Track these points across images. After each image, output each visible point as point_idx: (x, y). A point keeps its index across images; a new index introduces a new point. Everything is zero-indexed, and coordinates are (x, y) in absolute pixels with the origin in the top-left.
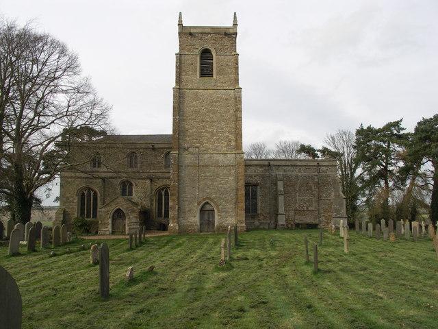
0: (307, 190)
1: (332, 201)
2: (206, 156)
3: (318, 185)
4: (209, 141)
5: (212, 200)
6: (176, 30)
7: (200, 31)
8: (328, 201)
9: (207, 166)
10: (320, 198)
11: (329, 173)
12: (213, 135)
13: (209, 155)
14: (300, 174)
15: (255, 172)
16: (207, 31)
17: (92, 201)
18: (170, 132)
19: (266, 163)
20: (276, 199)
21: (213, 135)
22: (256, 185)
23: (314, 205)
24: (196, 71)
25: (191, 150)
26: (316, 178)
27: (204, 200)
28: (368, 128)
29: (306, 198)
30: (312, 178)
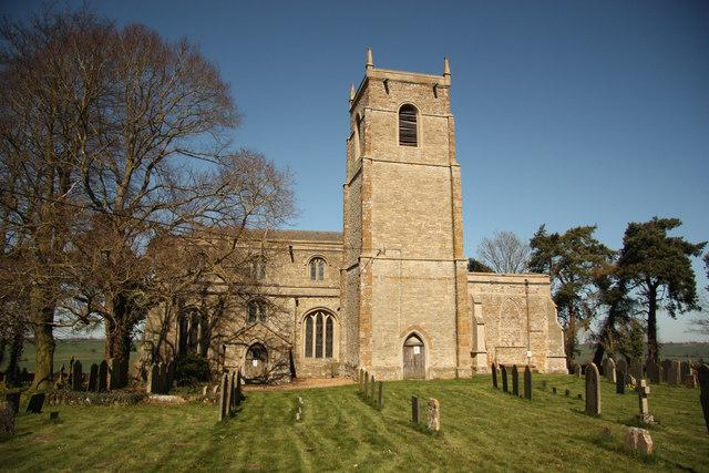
25: (389, 253)
26: (524, 301)
27: (410, 329)
29: (511, 330)
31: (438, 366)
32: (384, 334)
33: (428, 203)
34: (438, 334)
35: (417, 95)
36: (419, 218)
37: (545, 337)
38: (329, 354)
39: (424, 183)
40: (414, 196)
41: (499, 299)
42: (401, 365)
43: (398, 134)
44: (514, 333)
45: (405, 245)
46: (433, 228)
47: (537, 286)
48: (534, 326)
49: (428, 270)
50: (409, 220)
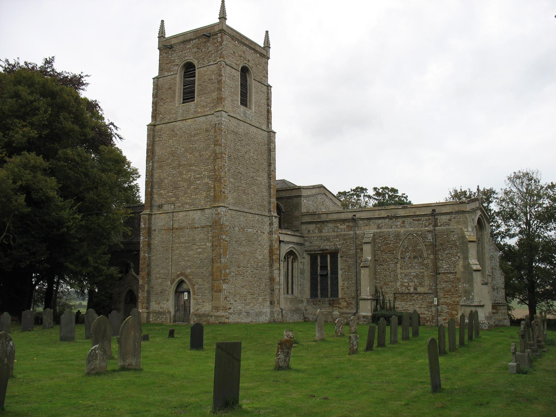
0: (415, 257)
1: (458, 276)
2: (181, 215)
3: (434, 248)
4: (186, 193)
5: (186, 277)
6: (155, 42)
7: (181, 39)
8: (451, 276)
9: (181, 228)
10: (436, 272)
11: (453, 226)
12: (190, 183)
13: (184, 213)
14: (402, 230)
15: (334, 231)
16: (188, 38)
17: (319, 288)
18: (277, 179)
19: (429, 211)
20: (358, 275)
21: (190, 183)
22: (334, 255)
23: (427, 282)
24: (174, 97)
25: (166, 207)
26: (430, 236)
27: (178, 276)
28: (125, 157)
29: (413, 272)
30: (423, 236)
31: (199, 312)
32: (160, 281)
33: (197, 154)
34: (200, 281)
35: (195, 50)
36: (189, 171)
37: (459, 279)
38: (292, 293)
39: (195, 136)
40: (186, 150)
41: (398, 235)
42: (172, 310)
43: (240, 93)
44: (417, 276)
45: (178, 198)
46: (198, 179)
47: (448, 217)
48: (444, 266)
49: (194, 219)
50: (181, 173)
